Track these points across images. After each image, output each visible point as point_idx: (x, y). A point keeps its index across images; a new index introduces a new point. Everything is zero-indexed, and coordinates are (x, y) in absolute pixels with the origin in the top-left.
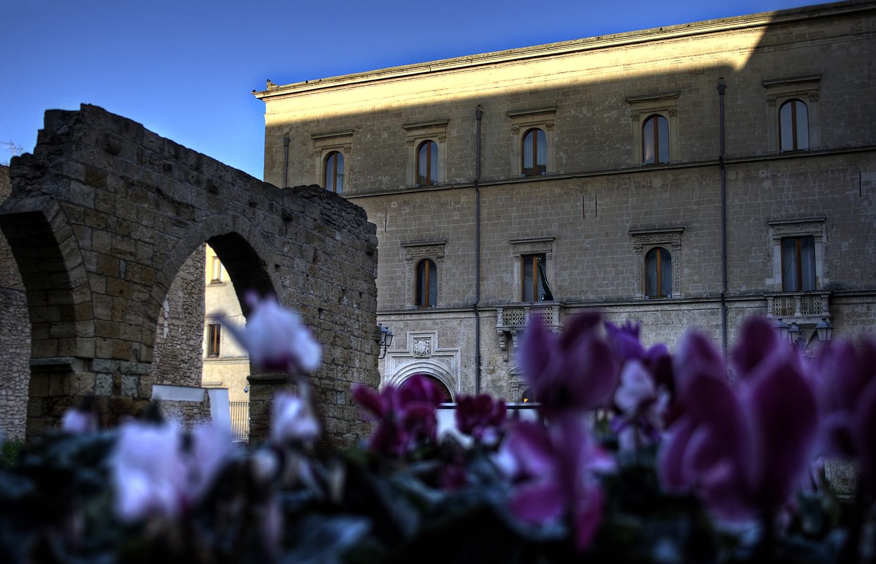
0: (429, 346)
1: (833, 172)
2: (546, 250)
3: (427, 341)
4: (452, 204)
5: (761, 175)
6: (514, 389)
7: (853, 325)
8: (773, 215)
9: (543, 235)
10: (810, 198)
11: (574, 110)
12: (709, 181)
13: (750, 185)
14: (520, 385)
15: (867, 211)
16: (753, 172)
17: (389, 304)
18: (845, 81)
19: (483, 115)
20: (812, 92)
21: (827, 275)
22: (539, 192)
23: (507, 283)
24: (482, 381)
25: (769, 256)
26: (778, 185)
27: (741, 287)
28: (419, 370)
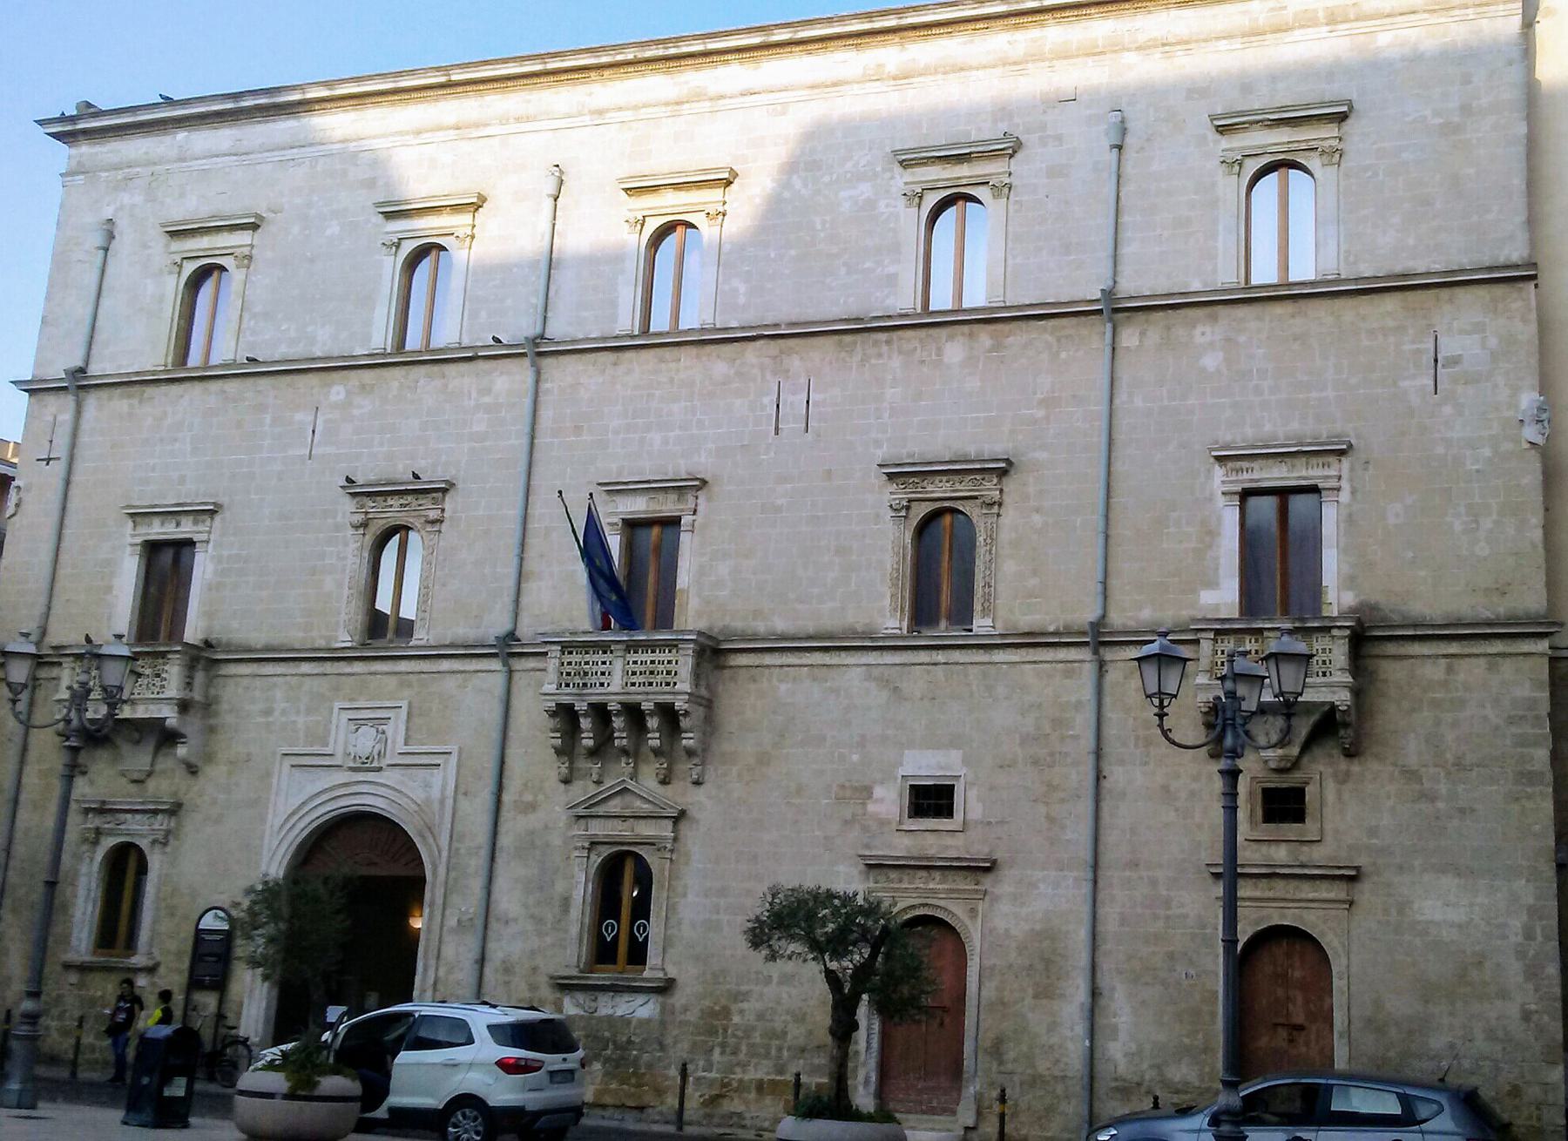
1: (1371, 333)
2: (682, 510)
4: (474, 395)
12: (1077, 351)
14: (592, 843)
17: (301, 634)
21: (1350, 582)
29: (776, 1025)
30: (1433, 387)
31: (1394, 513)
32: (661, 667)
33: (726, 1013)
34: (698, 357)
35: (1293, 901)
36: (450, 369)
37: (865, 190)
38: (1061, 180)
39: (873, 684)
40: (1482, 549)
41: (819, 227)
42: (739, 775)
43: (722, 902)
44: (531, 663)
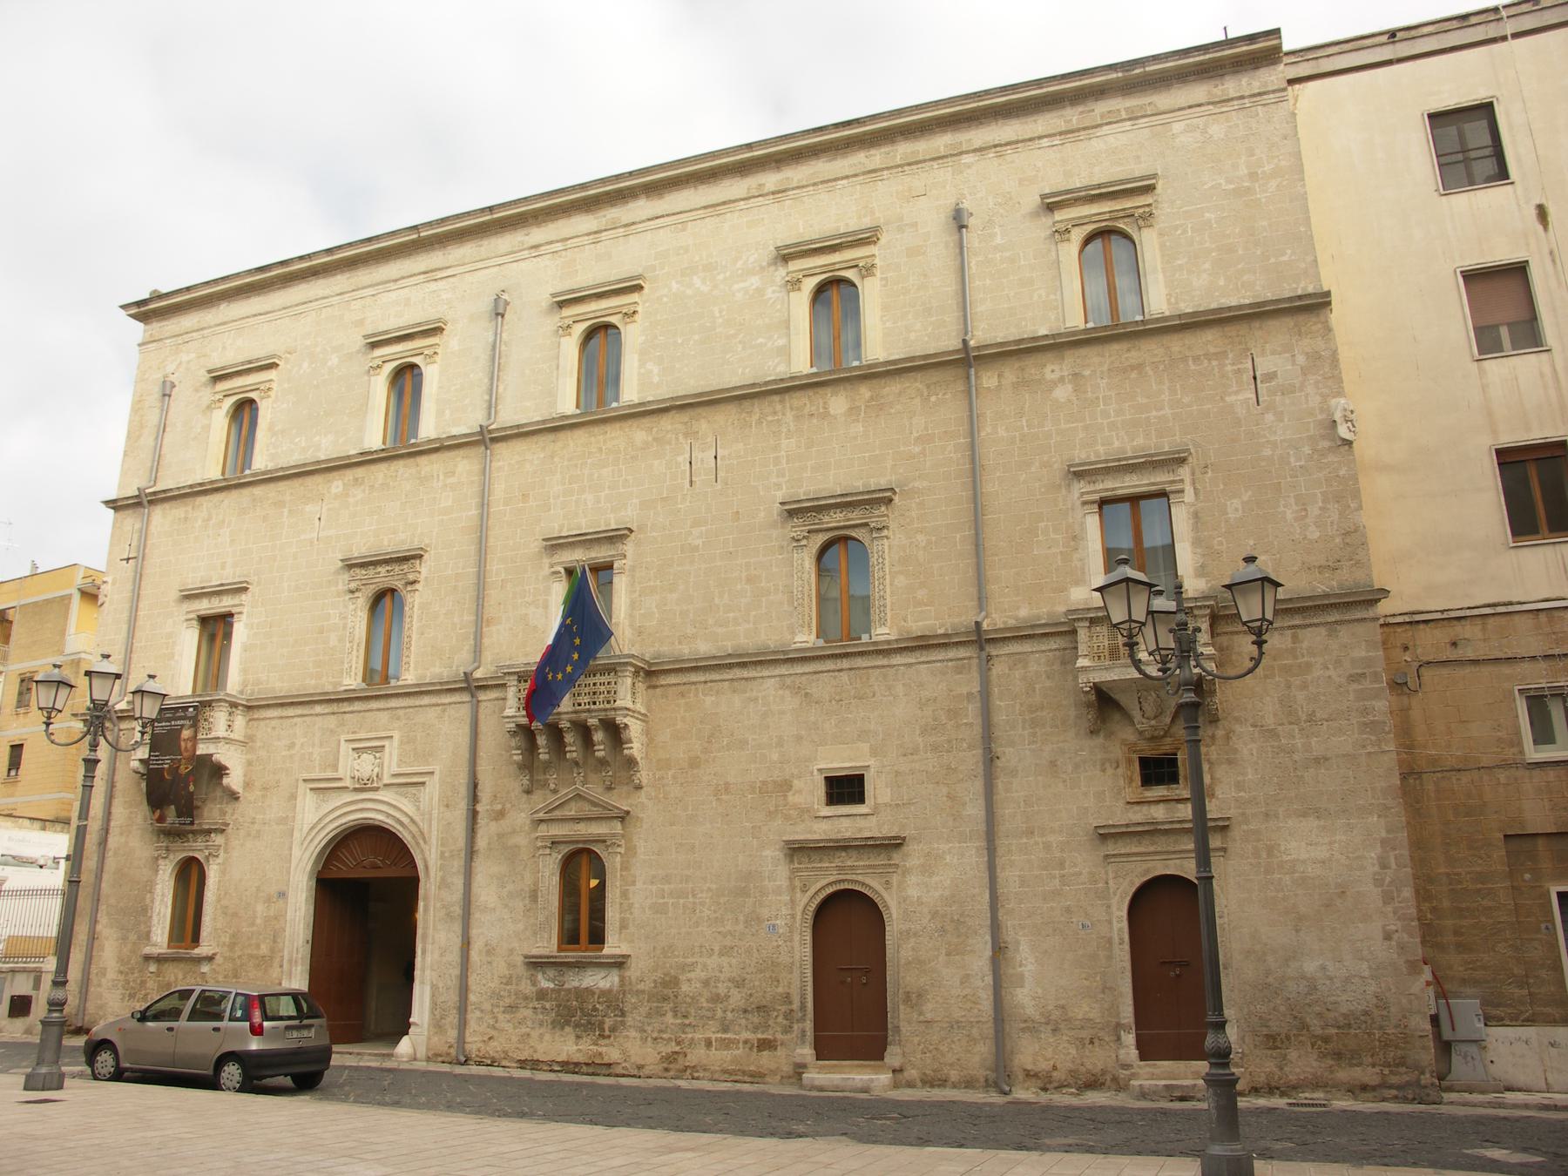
0: (381, 765)
1: (1196, 359)
2: (613, 556)
3: (378, 755)
4: (441, 477)
5: (1049, 376)
6: (541, 852)
7: (1266, 677)
8: (1081, 455)
9: (610, 524)
10: (1154, 413)
11: (677, 282)
12: (944, 394)
13: (1027, 396)
14: (553, 843)
15: (1275, 432)
16: (1033, 371)
17: (313, 682)
18: (1206, 187)
19: (508, 307)
20: (1141, 211)
21: (1201, 571)
22: (605, 441)
23: (536, 627)
24: (479, 836)
25: (1076, 538)
26: (1086, 392)
27: (1018, 608)
28: (344, 820)
29: (720, 991)
30: (1255, 399)
31: (1234, 508)
32: (602, 688)
33: (674, 982)
34: (621, 428)
35: (1174, 852)
36: (423, 460)
37: (755, 281)
38: (920, 258)
39: (787, 692)
40: (1314, 533)
41: (718, 315)
42: (674, 777)
43: (666, 887)
44: (493, 694)
